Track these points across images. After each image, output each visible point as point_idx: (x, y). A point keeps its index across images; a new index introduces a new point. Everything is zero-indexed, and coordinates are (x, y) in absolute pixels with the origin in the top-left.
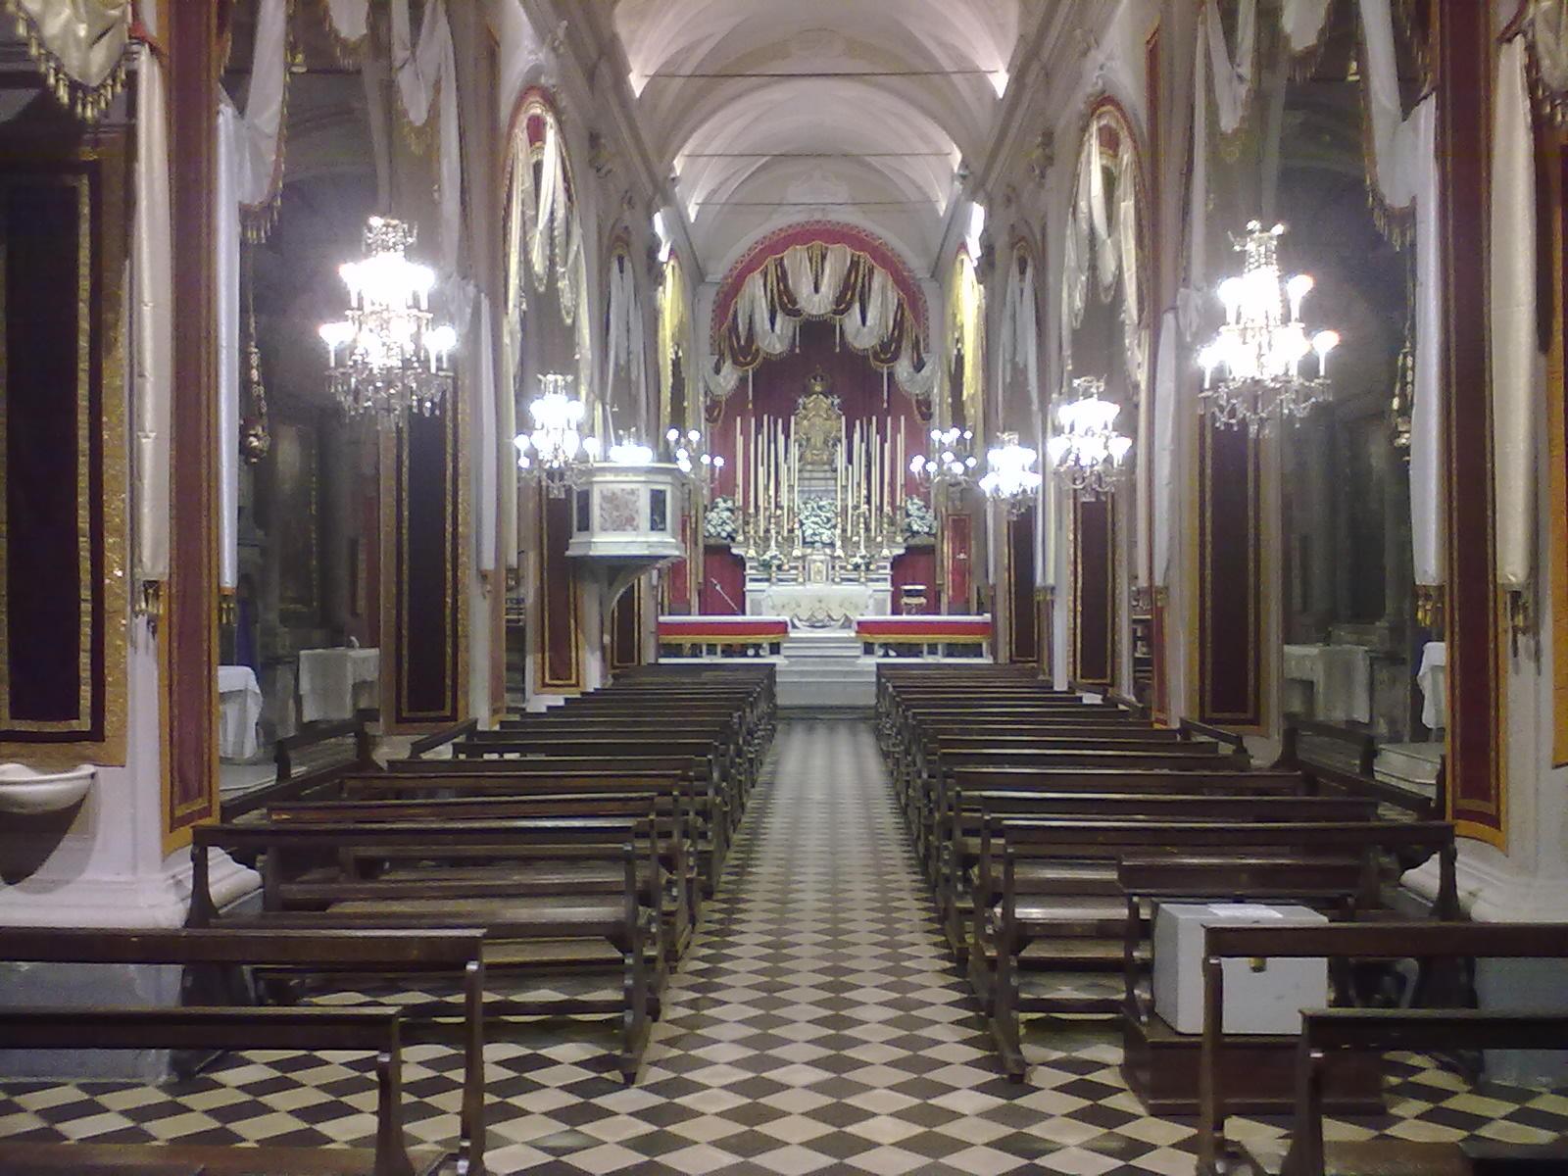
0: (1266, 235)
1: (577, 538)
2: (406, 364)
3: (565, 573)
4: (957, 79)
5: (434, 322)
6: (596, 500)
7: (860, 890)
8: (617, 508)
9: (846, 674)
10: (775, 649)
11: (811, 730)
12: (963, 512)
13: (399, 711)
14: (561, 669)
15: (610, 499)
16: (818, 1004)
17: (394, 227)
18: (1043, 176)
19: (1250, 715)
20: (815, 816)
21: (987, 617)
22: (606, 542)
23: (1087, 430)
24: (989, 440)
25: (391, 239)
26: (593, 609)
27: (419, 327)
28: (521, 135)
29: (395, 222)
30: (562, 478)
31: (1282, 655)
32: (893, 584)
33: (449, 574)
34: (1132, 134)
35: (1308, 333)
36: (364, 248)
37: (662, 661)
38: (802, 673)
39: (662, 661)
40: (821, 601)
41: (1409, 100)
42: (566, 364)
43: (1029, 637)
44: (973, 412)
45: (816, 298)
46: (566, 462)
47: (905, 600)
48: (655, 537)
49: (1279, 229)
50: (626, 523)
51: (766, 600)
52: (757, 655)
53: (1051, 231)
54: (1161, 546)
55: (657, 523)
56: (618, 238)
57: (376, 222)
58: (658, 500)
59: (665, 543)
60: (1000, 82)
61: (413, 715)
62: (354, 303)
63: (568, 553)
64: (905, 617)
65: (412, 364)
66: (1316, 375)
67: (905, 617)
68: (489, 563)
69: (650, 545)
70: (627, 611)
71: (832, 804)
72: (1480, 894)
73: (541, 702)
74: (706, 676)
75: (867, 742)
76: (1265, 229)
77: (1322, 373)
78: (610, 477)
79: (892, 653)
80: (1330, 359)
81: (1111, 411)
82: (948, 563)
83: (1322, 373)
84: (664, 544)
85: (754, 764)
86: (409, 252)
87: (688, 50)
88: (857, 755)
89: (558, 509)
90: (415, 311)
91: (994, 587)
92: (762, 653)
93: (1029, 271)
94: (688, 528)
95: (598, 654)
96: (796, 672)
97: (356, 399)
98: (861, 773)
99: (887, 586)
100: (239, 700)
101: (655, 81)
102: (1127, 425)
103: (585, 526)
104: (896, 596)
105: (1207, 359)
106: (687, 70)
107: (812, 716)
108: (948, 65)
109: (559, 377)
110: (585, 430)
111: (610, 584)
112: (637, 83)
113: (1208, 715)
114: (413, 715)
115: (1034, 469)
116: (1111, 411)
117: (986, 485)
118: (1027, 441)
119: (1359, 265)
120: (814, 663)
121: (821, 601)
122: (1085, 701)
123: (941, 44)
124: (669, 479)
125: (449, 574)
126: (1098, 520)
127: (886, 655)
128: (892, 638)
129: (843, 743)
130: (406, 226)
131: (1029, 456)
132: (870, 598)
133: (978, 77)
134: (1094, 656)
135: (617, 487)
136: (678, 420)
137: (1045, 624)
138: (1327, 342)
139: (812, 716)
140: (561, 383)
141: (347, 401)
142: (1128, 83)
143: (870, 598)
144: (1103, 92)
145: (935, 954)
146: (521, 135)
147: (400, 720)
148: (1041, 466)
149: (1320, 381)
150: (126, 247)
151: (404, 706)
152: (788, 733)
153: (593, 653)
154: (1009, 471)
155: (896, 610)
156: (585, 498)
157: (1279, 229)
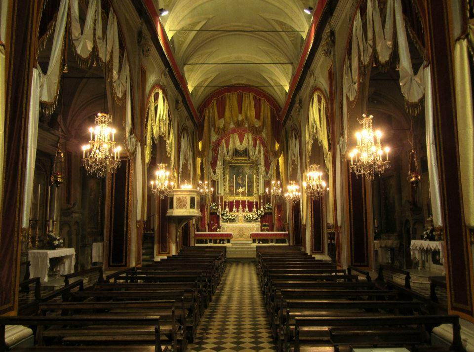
0: (368, 118)
1: (170, 211)
2: (106, 158)
3: (168, 221)
4: (275, 88)
5: (116, 145)
6: (175, 200)
7: (247, 325)
8: (181, 202)
9: (248, 248)
10: (228, 241)
11: (237, 265)
12: (281, 203)
13: (159, 251)
14: (164, 249)
15: (179, 199)
16: (251, 338)
17: (105, 117)
18: (299, 111)
19: (366, 264)
20: (236, 295)
21: (287, 232)
22: (177, 212)
23: (314, 177)
24: (287, 183)
25: (103, 120)
26: (174, 232)
27: (111, 146)
28: (152, 99)
29: (105, 115)
30: (164, 193)
31: (373, 243)
32: (261, 223)
33: (125, 221)
34: (325, 97)
35: (382, 148)
36: (95, 122)
37: (197, 245)
38: (236, 248)
39: (197, 245)
40: (241, 228)
41: (416, 68)
42: (166, 160)
43: (299, 239)
44: (283, 175)
45: (242, 146)
46: (165, 189)
47: (263, 228)
48: (192, 210)
49: (371, 117)
50: (184, 206)
51: (226, 228)
52: (223, 243)
53: (302, 125)
54: (336, 212)
55: (192, 206)
56: (184, 129)
57: (99, 114)
58: (192, 199)
59: (195, 212)
60: (287, 88)
61: (113, 264)
62: (92, 139)
63: (167, 215)
64: (263, 232)
65: (110, 157)
66: (386, 160)
67: (263, 232)
68: (139, 218)
69: (190, 213)
70: (186, 230)
71: (241, 291)
72: (468, 341)
73: (158, 259)
74: (207, 250)
75: (253, 269)
76: (368, 116)
77: (387, 159)
78: (179, 193)
79: (261, 242)
80: (389, 156)
81: (321, 174)
82: (276, 217)
83: (387, 159)
84: (194, 212)
85: (219, 279)
86: (109, 124)
87: (205, 81)
88: (250, 273)
89: (166, 202)
90: (110, 141)
91: (289, 224)
92: (225, 242)
93: (297, 140)
94: (202, 207)
95: (175, 244)
96: (234, 248)
97: (91, 168)
98: (251, 280)
99: (259, 223)
100: (69, 260)
101: (195, 88)
102: (326, 177)
103: (172, 207)
104: (261, 226)
105: (352, 154)
106: (205, 85)
107: (239, 261)
108: (273, 84)
109: (164, 165)
110: (170, 179)
111: (179, 224)
112: (190, 88)
113: (354, 264)
114: (113, 264)
115: (299, 191)
116: (321, 174)
117: (286, 195)
118: (297, 182)
119: (402, 121)
120: (240, 245)
121: (241, 228)
122: (316, 259)
123: (272, 80)
124: (195, 194)
125: (125, 221)
126: (318, 202)
127: (259, 243)
128: (261, 238)
129: (246, 269)
130: (108, 116)
131: (297, 187)
132: (255, 227)
133: (282, 87)
134: (317, 247)
135: (181, 196)
136: (202, 178)
137: (325, 209)
138: (388, 150)
139: (239, 261)
140: (164, 166)
141: (88, 168)
142: (324, 83)
143: (255, 227)
144: (316, 87)
145: (270, 346)
146: (152, 99)
147: (109, 266)
148: (301, 190)
149: (387, 162)
150: (342, 219)
151: (111, 262)
152: (231, 266)
153: (174, 244)
154: (292, 191)
155: (261, 231)
156: (172, 199)
157: (371, 117)
